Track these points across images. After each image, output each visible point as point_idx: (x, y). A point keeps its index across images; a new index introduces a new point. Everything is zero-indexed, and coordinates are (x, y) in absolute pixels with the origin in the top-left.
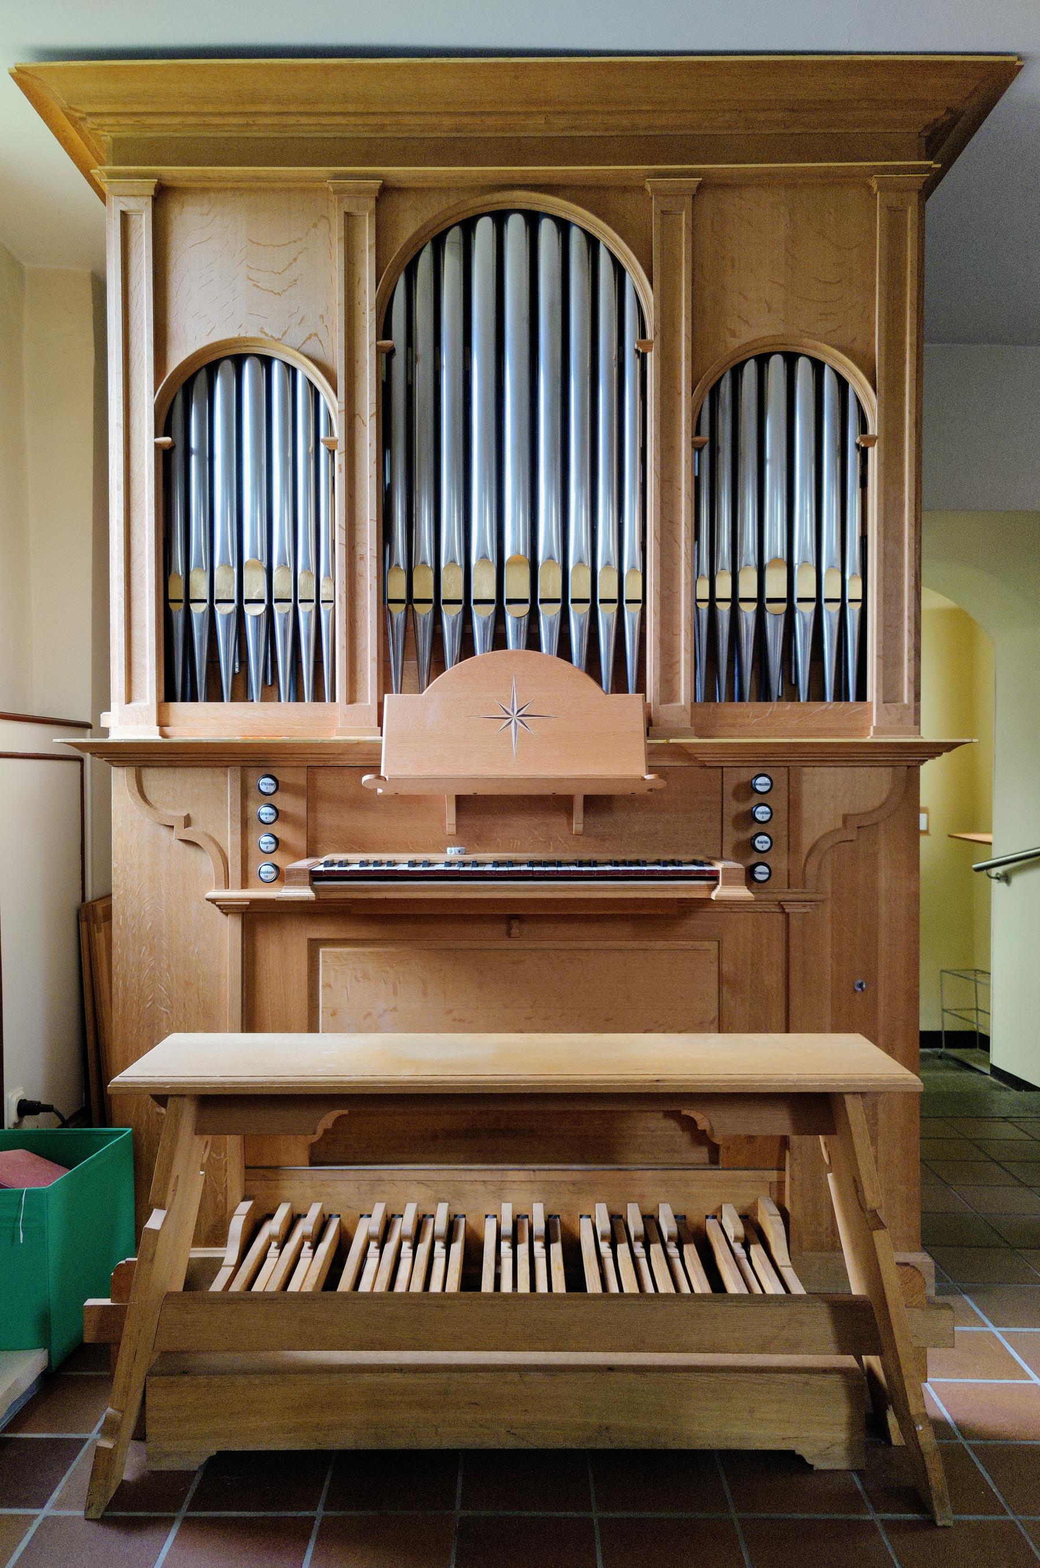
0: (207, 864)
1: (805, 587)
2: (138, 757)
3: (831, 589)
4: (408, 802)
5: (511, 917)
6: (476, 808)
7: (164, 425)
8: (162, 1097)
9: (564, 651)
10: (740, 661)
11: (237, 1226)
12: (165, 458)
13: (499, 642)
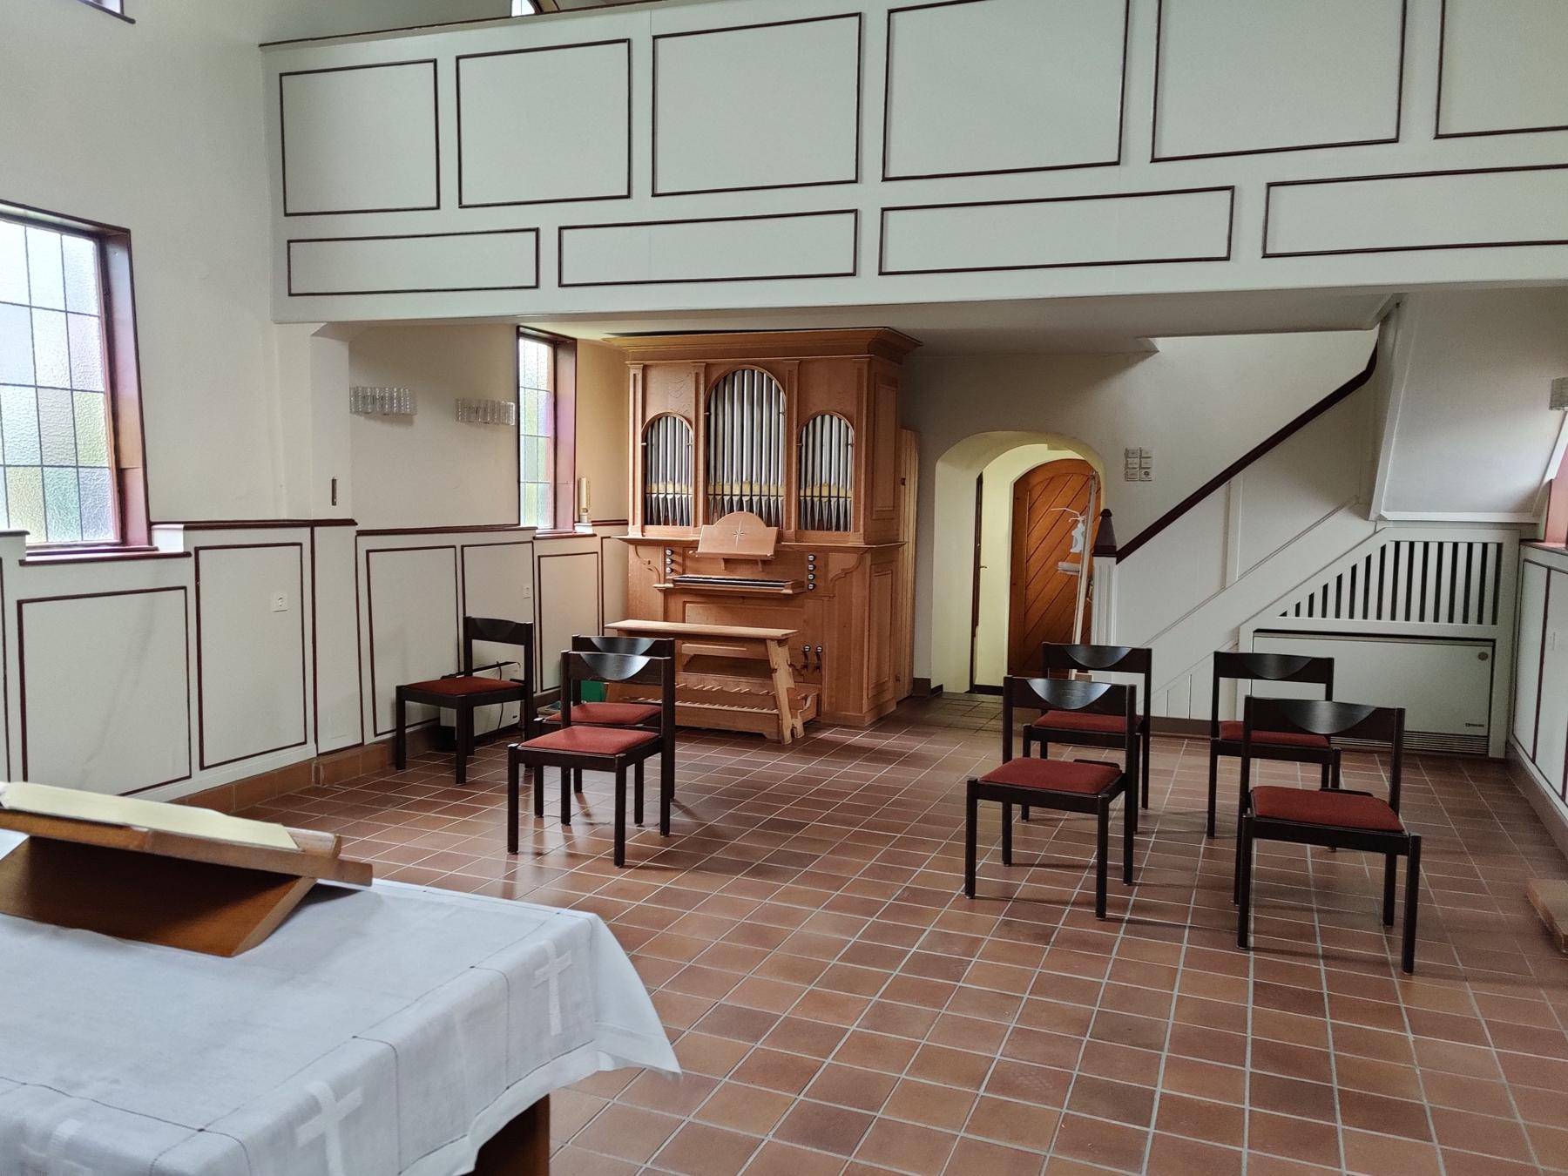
0: (655, 576)
1: (834, 493)
3: (842, 494)
4: (710, 558)
5: (743, 597)
6: (730, 562)
7: (645, 439)
9: (751, 510)
10: (812, 516)
12: (645, 449)
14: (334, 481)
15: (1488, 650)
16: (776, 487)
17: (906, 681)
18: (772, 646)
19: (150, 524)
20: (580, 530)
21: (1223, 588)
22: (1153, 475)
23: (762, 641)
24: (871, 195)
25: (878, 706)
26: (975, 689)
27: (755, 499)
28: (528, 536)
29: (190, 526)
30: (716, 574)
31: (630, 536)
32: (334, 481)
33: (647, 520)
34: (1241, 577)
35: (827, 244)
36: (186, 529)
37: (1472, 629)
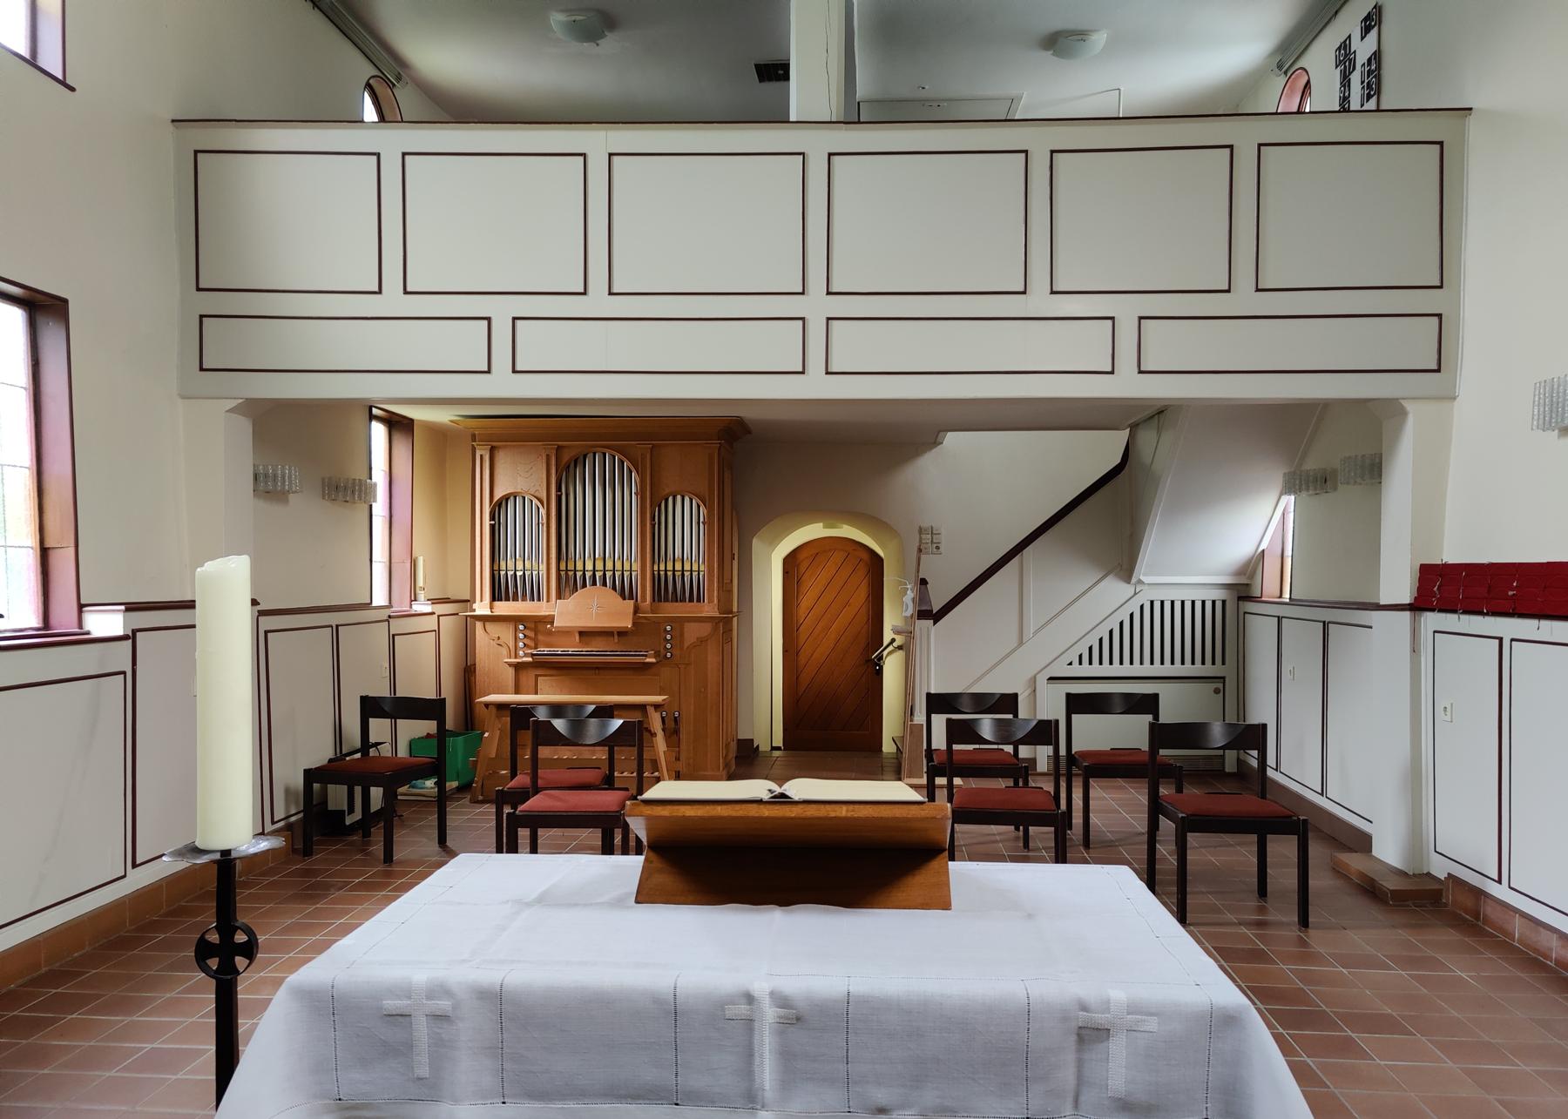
0: (504, 651)
2: (484, 619)
4: (565, 632)
6: (585, 634)
7: (492, 518)
9: (604, 584)
10: (664, 590)
12: (492, 527)
13: (594, 583)
16: (630, 560)
17: (734, 746)
18: (651, 710)
19: (81, 607)
20: (419, 608)
21: (1021, 643)
22: (942, 547)
23: (642, 707)
24: (816, 306)
25: (727, 765)
26: (774, 748)
27: (609, 574)
29: (131, 608)
30: (570, 648)
31: (478, 612)
34: (1036, 633)
35: (779, 346)
36: (127, 610)
37: (1208, 670)
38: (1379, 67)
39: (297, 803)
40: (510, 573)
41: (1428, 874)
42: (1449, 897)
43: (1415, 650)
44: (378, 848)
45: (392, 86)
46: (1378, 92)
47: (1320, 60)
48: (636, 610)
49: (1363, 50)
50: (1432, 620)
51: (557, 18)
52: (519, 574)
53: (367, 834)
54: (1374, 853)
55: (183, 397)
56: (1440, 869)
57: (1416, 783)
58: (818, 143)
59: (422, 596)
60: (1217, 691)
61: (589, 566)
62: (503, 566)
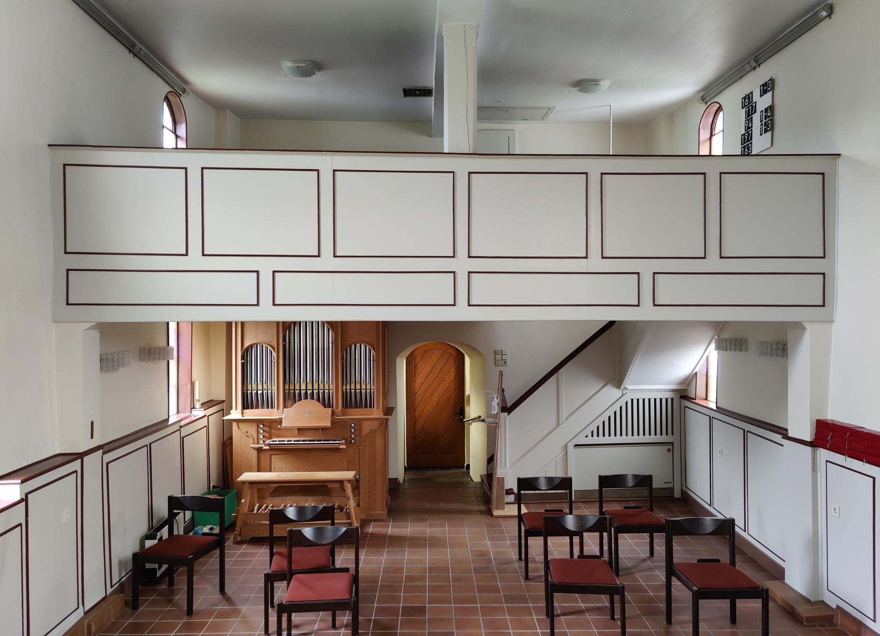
0: (251, 440)
4: (289, 429)
6: (301, 430)
7: (243, 358)
8: (243, 482)
9: (312, 398)
10: (351, 401)
11: (256, 508)
12: (243, 364)
14: (92, 423)
15: (671, 447)
16: (330, 385)
21: (558, 425)
22: (508, 363)
24: (462, 265)
27: (315, 392)
28: (177, 427)
32: (92, 423)
33: (246, 405)
35: (438, 289)
37: (664, 438)
38: (772, 115)
39: (126, 569)
40: (254, 392)
41: (822, 601)
42: (839, 620)
43: (814, 470)
44: (181, 597)
45: (179, 96)
46: (772, 129)
47: (731, 98)
48: (333, 414)
49: (762, 102)
50: (824, 454)
51: (288, 64)
52: (260, 392)
53: (171, 583)
54: (786, 581)
55: (55, 322)
56: (833, 602)
57: (815, 548)
58: (462, 166)
59: (198, 405)
60: (669, 450)
61: (303, 387)
62: (249, 387)
